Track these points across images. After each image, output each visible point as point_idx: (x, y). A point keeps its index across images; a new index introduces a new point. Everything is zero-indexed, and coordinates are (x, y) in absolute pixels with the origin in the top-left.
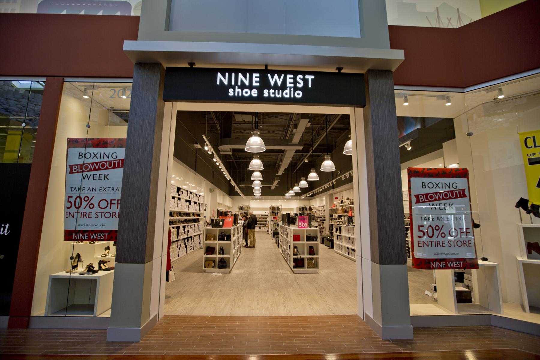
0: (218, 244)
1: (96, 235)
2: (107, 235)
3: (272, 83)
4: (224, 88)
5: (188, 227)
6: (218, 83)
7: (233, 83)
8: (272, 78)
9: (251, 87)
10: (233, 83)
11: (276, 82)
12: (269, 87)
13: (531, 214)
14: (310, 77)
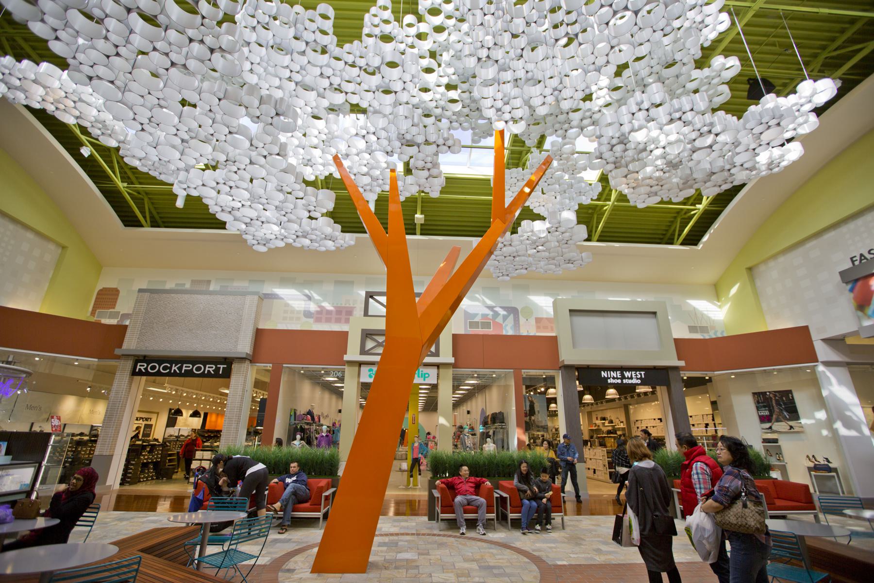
9: (617, 378)
10: (609, 376)
12: (626, 378)
14: (643, 373)
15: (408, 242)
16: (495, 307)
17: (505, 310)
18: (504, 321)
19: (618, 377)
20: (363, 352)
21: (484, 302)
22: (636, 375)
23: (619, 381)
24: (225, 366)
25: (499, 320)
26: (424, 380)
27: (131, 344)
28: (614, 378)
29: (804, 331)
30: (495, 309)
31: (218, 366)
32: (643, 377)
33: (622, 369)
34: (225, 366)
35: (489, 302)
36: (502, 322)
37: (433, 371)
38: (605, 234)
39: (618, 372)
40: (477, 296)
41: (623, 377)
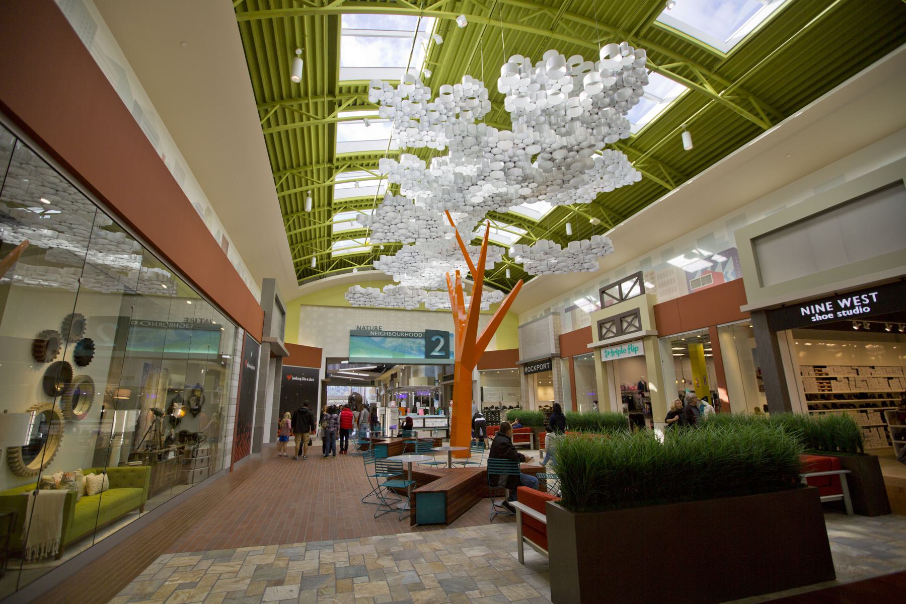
0: (689, 70)
1: (494, 283)
2: (591, 341)
3: (843, 306)
4: (808, 317)
5: (202, 452)
6: (803, 314)
7: (813, 312)
8: (841, 301)
9: (827, 312)
10: (813, 312)
11: (845, 305)
12: (841, 309)
13: (347, 402)
14: (873, 294)
15: (122, 411)
16: (712, 256)
17: (723, 256)
18: (723, 269)
19: (829, 309)
20: (601, 337)
21: (701, 255)
22: (862, 300)
23: (831, 316)
24: (877, 293)
25: (719, 269)
26: (636, 353)
27: (522, 358)
28: (821, 313)
29: (319, 351)
30: (713, 258)
31: (870, 294)
32: (875, 300)
33: (834, 297)
34: (877, 293)
35: (706, 253)
36: (721, 271)
37: (639, 344)
38: (700, 143)
39: (827, 304)
40: (694, 251)
41: (837, 308)
